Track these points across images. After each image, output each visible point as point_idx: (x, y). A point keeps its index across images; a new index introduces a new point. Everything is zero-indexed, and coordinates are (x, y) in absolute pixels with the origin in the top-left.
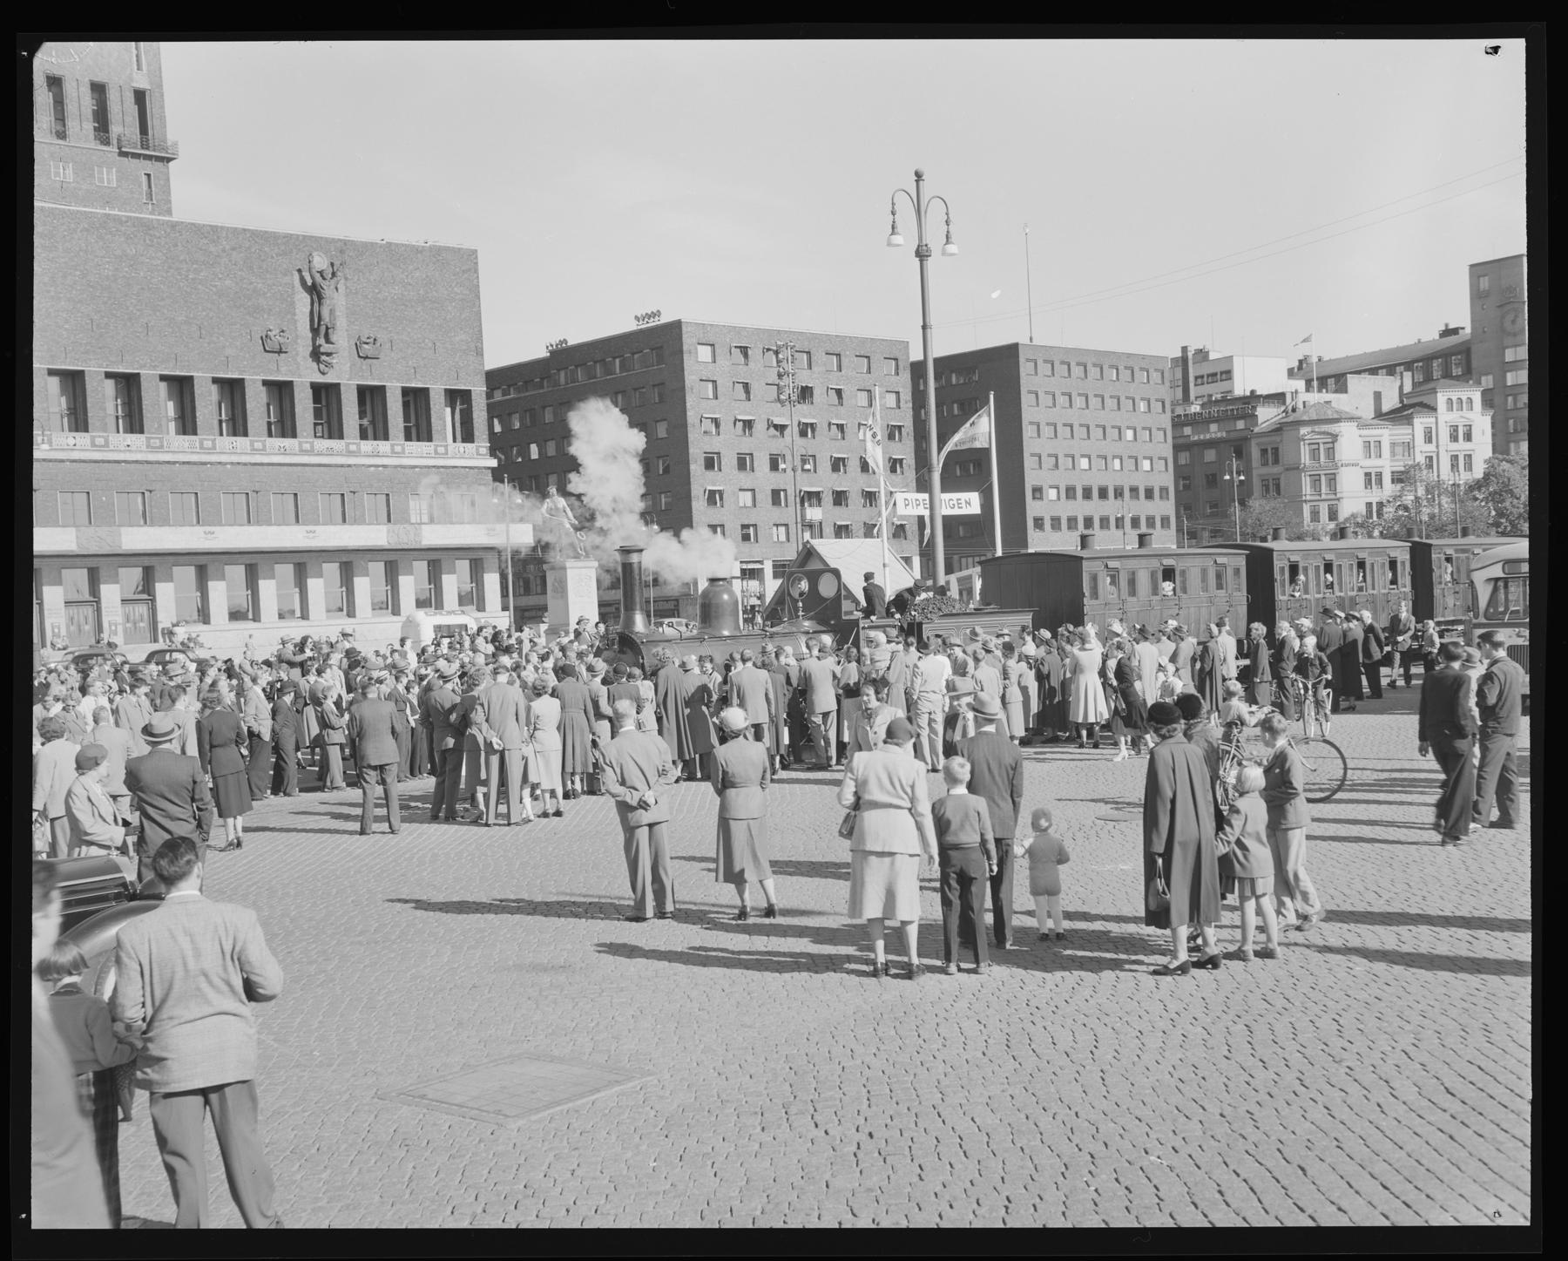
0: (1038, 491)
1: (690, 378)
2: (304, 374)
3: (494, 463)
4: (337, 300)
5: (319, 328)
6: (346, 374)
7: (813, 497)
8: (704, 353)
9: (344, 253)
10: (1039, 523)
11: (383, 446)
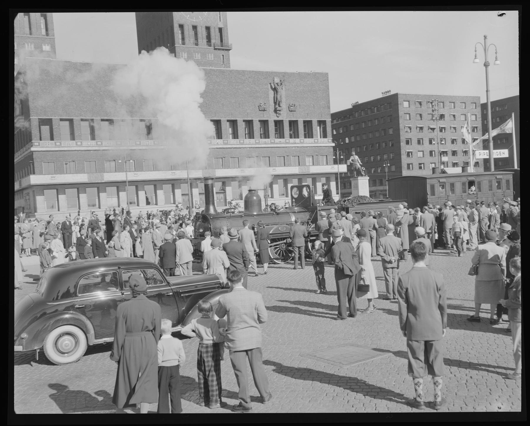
1: (401, 113)
2: (272, 118)
3: (334, 145)
4: (283, 92)
5: (277, 102)
6: (285, 117)
7: (444, 153)
8: (406, 104)
9: (284, 76)
11: (297, 140)
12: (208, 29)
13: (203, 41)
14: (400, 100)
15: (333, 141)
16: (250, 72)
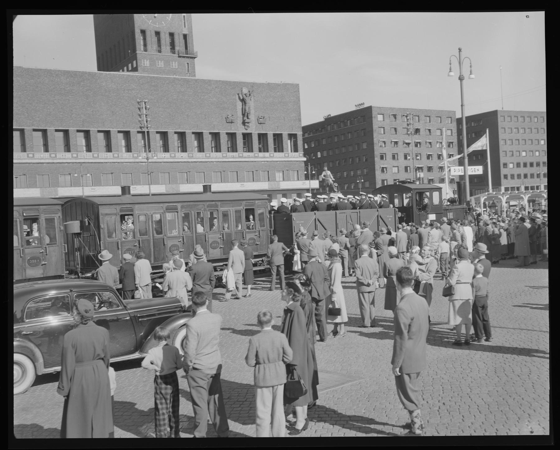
0: (505, 165)
1: (375, 127)
2: (240, 130)
3: (305, 159)
4: (251, 104)
5: (245, 114)
6: (254, 129)
7: (420, 169)
8: (380, 117)
9: (253, 86)
10: (506, 177)
11: (267, 154)
12: (172, 35)
13: (166, 48)
14: (374, 113)
15: (305, 156)
16: (217, 81)
